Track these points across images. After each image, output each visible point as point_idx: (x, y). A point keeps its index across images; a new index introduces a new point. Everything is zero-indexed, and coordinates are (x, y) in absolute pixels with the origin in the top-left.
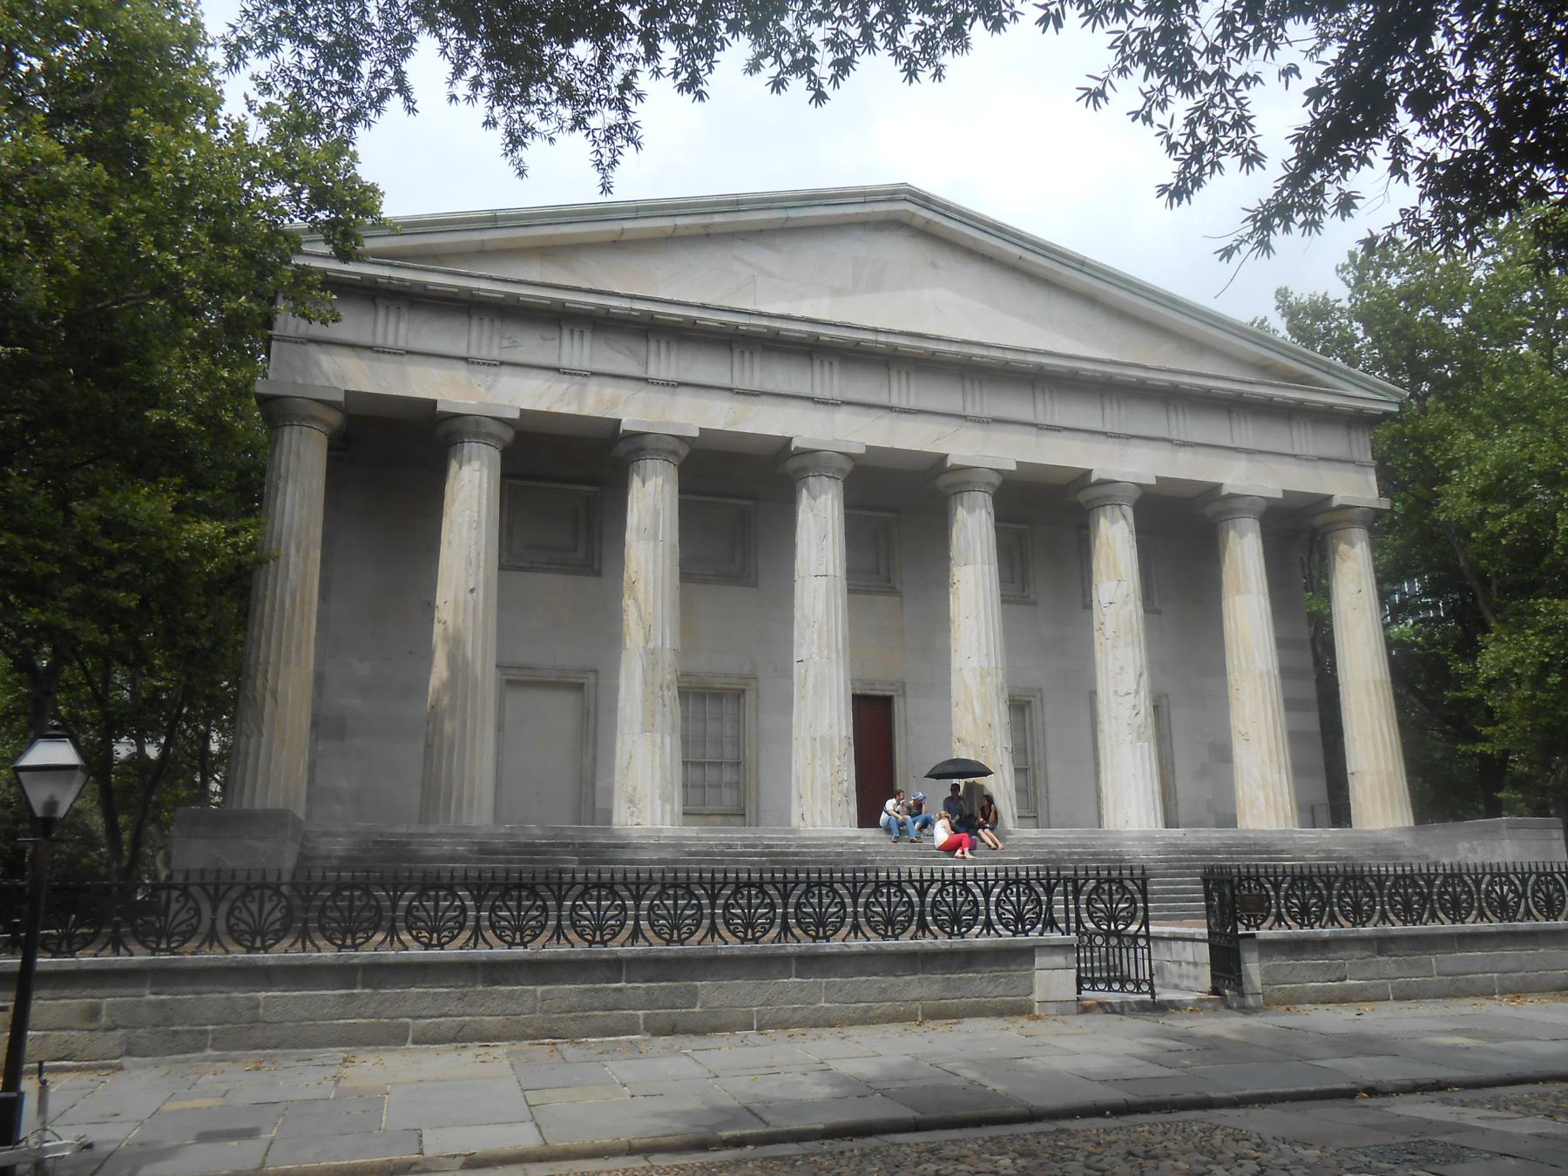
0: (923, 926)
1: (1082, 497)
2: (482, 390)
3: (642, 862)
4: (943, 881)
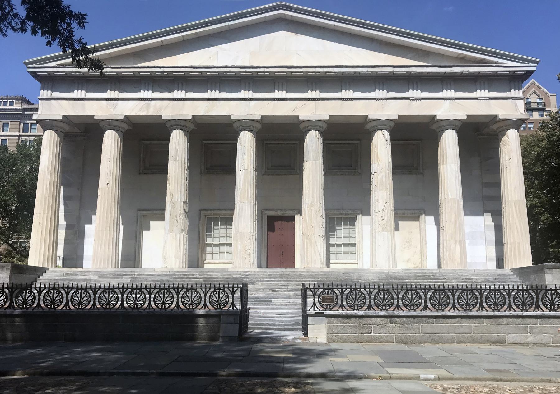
0: (482, 306)
1: (434, 127)
2: (112, 110)
3: (79, 280)
4: (215, 288)
